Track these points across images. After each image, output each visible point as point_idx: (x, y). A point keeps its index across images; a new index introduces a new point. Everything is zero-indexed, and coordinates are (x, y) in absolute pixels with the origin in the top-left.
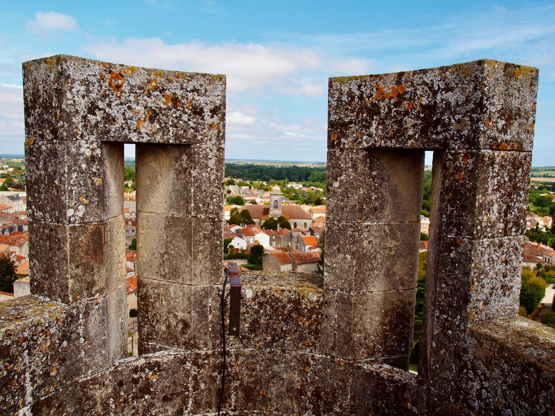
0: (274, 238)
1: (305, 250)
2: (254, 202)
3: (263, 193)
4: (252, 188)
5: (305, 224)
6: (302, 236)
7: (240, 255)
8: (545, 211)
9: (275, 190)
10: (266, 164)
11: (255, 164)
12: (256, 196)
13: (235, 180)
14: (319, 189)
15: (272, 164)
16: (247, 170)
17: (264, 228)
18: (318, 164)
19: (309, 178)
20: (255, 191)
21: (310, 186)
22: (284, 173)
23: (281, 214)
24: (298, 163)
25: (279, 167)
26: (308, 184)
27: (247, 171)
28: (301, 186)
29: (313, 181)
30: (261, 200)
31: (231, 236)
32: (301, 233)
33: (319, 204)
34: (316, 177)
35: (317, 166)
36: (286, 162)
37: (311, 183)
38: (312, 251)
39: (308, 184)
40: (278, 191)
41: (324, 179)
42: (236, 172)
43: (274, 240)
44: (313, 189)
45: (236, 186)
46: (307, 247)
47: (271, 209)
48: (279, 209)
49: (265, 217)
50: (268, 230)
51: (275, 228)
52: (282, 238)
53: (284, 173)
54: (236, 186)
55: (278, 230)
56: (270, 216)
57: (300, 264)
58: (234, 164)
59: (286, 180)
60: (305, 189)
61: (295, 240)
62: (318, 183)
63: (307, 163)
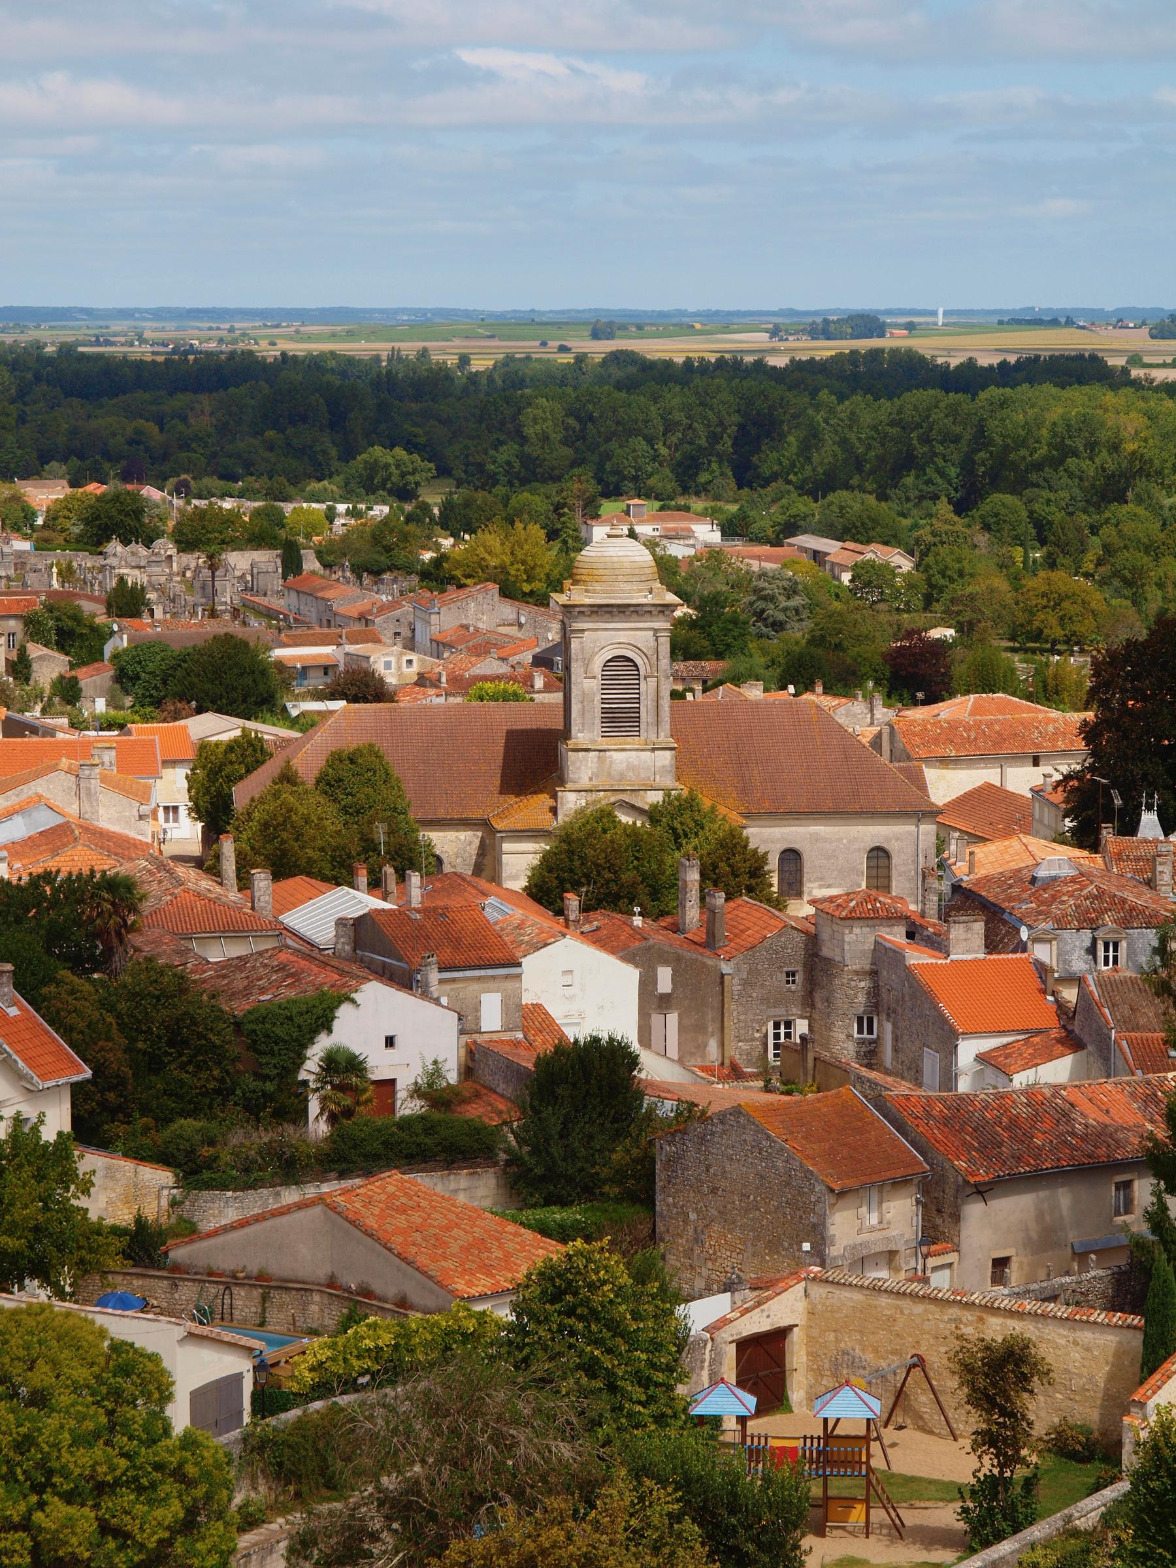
0: (665, 979)
1: (949, 1077)
2: (361, 687)
3: (425, 609)
4: (311, 564)
5: (879, 856)
6: (917, 957)
7: (437, 1137)
8: (897, 839)
9: (615, 573)
10: (360, 348)
11: (267, 351)
12: (364, 626)
13: (151, 492)
14: (874, 553)
15: (409, 348)
16: (205, 402)
17: (572, 901)
18: (823, 329)
19: (768, 460)
20: (347, 596)
21: (791, 528)
22: (543, 417)
23: (669, 782)
24: (640, 324)
25: (479, 365)
26: (766, 517)
27: (204, 413)
28: (707, 533)
29: (818, 489)
30: (418, 663)
31: (326, 978)
32: (896, 936)
33: (379, 701)
34: (826, 454)
35: (824, 350)
36: (530, 323)
37: (803, 505)
38: (1021, 1080)
39: (766, 517)
40: (634, 576)
41: (907, 462)
42: (110, 422)
43: (664, 1003)
44: (817, 556)
45: (166, 546)
46: (968, 1051)
47: (580, 736)
48: (648, 733)
49: (532, 809)
50: (599, 919)
51: (658, 895)
52: (734, 986)
53: (543, 417)
54: (166, 546)
55: (692, 914)
56: (571, 802)
57: (982, 1191)
58: (67, 351)
59: (580, 483)
60: (755, 560)
61: (852, 993)
62: (856, 502)
63: (725, 322)
